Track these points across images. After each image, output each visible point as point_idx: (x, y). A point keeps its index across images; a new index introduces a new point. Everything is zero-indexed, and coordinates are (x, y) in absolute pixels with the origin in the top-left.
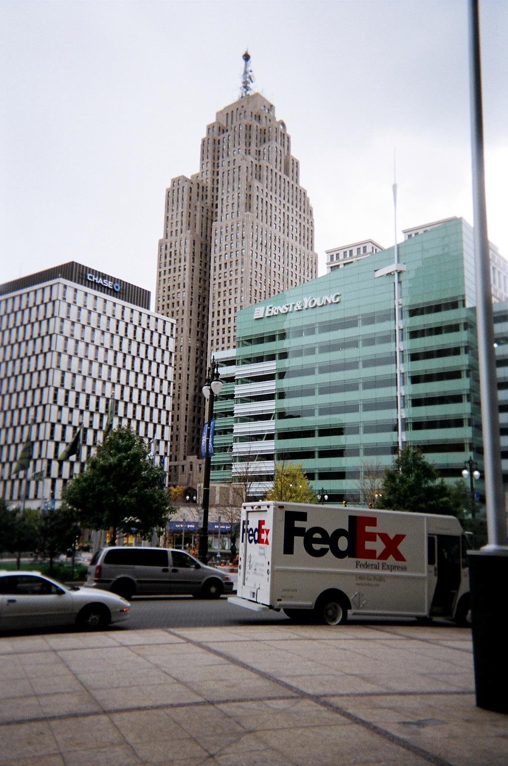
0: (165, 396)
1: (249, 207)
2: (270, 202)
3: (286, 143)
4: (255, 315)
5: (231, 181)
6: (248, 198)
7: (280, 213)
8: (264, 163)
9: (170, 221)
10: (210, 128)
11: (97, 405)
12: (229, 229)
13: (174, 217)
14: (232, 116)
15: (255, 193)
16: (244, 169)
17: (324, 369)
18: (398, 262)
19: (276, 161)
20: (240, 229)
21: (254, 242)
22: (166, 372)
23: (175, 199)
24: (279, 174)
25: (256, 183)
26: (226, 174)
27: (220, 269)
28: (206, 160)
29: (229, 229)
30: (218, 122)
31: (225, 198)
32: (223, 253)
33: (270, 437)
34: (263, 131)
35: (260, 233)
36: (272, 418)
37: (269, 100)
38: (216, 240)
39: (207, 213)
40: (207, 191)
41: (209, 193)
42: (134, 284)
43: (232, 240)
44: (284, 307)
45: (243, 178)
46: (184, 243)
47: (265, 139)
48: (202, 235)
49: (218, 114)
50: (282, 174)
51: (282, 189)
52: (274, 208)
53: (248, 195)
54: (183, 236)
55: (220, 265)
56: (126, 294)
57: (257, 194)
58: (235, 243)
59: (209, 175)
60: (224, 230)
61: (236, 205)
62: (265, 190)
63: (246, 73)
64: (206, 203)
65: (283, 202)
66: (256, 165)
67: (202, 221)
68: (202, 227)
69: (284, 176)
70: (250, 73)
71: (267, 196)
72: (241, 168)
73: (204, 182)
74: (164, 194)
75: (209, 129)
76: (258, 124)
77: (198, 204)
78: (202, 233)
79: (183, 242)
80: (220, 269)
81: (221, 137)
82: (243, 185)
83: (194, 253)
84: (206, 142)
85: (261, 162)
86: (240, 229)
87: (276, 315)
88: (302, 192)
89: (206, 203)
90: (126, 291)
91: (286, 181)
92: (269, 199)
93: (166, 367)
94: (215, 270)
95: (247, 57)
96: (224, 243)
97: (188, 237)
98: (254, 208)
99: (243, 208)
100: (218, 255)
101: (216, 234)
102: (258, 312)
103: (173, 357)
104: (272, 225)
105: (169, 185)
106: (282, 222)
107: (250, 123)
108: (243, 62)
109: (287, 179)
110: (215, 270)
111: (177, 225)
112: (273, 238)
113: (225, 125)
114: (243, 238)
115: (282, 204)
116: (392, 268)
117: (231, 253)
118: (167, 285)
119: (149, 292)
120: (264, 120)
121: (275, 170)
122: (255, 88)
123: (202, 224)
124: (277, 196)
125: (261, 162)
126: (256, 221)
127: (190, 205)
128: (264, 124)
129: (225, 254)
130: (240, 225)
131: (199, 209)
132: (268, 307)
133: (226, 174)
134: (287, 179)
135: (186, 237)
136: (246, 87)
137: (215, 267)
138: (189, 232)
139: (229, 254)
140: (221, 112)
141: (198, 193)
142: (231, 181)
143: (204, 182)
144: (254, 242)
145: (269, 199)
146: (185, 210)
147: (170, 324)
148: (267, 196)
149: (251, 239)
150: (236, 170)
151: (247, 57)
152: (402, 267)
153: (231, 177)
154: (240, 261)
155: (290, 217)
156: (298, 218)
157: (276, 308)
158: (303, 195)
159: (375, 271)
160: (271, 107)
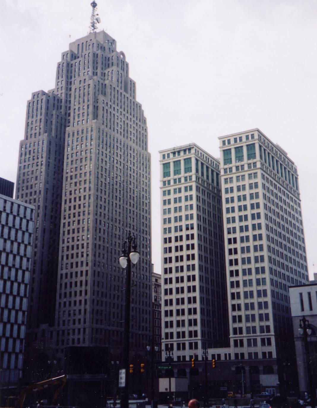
5: (82, 95)
10: (64, 55)
15: (101, 106)
16: (92, 86)
24: (120, 91)
25: (101, 98)
26: (78, 90)
28: (60, 79)
38: (68, 140)
41: (63, 104)
45: (91, 92)
48: (57, 137)
50: (122, 91)
59: (64, 91)
62: (109, 103)
63: (93, 16)
64: (61, 112)
66: (102, 84)
69: (124, 93)
77: (54, 112)
78: (57, 136)
79: (41, 143)
88: (138, 106)
95: (94, 5)
96: (75, 143)
99: (91, 116)
105: (30, 97)
113: (76, 52)
114: (91, 140)
127: (47, 113)
131: (54, 116)
133: (78, 90)
138: (46, 134)
140: (74, 43)
141: (54, 104)
146: (43, 117)
150: (86, 87)
151: (94, 5)
153: (82, 92)
160: (113, 42)
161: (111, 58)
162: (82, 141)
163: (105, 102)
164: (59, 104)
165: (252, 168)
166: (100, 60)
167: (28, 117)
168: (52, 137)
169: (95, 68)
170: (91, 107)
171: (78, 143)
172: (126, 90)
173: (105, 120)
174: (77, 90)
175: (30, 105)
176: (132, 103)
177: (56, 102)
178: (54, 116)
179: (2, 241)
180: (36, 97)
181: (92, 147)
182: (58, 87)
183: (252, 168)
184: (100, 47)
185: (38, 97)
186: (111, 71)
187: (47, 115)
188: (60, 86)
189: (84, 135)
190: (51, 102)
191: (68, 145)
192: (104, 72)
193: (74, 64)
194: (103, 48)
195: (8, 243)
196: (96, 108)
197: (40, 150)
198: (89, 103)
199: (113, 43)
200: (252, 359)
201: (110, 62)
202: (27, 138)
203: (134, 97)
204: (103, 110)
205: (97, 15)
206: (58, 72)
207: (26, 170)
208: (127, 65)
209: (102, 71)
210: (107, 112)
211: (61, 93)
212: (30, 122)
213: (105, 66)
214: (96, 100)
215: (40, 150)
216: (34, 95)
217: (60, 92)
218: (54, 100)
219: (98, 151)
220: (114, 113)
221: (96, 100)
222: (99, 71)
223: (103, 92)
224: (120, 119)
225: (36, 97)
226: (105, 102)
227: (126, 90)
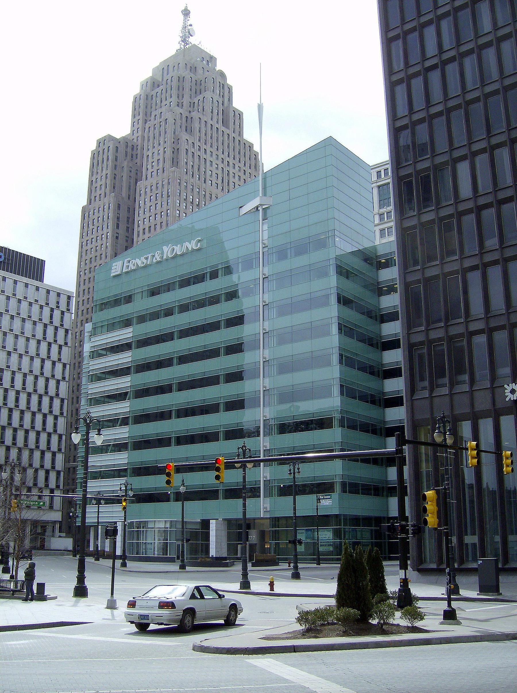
0: (58, 382)
1: (175, 162)
2: (209, 158)
3: (226, 94)
4: (112, 271)
5: (157, 135)
6: (175, 153)
7: (217, 168)
8: (195, 115)
9: (94, 185)
10: (144, 85)
11: (28, 402)
12: (154, 188)
13: (99, 180)
14: (168, 70)
15: (183, 146)
16: (171, 121)
17: (186, 333)
18: (265, 194)
19: (212, 112)
20: (166, 187)
21: (182, 200)
22: (60, 353)
23: (100, 162)
24: (216, 126)
25: (185, 136)
26: (152, 129)
27: (144, 233)
28: (137, 118)
29: (154, 188)
30: (152, 78)
31: (150, 155)
32: (147, 215)
33: (125, 422)
34: (181, 79)
35: (183, 187)
36: (127, 398)
37: (208, 52)
38: (140, 201)
39: (137, 174)
40: (137, 149)
42: (12, 248)
43: (156, 200)
44: (143, 259)
45: (170, 131)
46: (108, 208)
47: (201, 90)
48: (129, 198)
49: (154, 70)
50: (220, 126)
51: (226, 144)
52: (208, 163)
53: (176, 149)
54: (106, 200)
55: (144, 229)
56: (12, 264)
57: (187, 147)
58: (159, 203)
60: (148, 190)
61: (161, 161)
62: (197, 144)
63: (185, 27)
64: (137, 163)
65: (221, 156)
66: (187, 117)
67: (130, 182)
68: (129, 189)
69: (223, 129)
70: (189, 27)
71: (199, 150)
72: (167, 121)
73: (135, 140)
74: (89, 156)
75: (142, 86)
76: (192, 75)
77: (125, 164)
78: (129, 196)
79: (106, 207)
80: (144, 233)
81: (154, 93)
82: (169, 137)
83: (118, 218)
84: (138, 99)
85: (193, 114)
86: (166, 187)
87: (135, 270)
88: (247, 146)
89: (137, 163)
90: (12, 260)
91: (225, 134)
92: (202, 153)
93: (60, 347)
94: (138, 235)
95: (186, 13)
96: (148, 204)
97: (112, 200)
98: (182, 163)
99: (168, 163)
100: (141, 218)
101: (140, 195)
102: (115, 267)
103: (70, 335)
104: (207, 181)
105: (94, 146)
106: (220, 179)
107: (183, 75)
108: (182, 17)
109: (227, 131)
110: (138, 235)
111: (101, 189)
112: (208, 196)
113: (161, 80)
114: (168, 196)
115: (220, 158)
116: (256, 202)
117: (155, 215)
118: (88, 257)
119: (45, 261)
120: (200, 71)
121: (210, 122)
122: (192, 40)
123: (130, 186)
124: (214, 150)
125: (193, 114)
126: (185, 177)
127: (116, 166)
128: (200, 75)
129: (150, 217)
130: (166, 181)
131: (125, 169)
132: (126, 261)
133: (152, 129)
134: (227, 131)
135: (110, 200)
136: (184, 40)
137: (139, 232)
138: (113, 194)
139: (153, 216)
141: (126, 152)
142: (157, 135)
143: (135, 140)
144: (182, 200)
145: (202, 153)
146: (109, 172)
147: (66, 297)
148: (199, 150)
149: (178, 197)
150: (163, 124)
151: (186, 13)
152: (268, 201)
153: (157, 131)
154: (164, 224)
155: (231, 173)
156: (241, 174)
157: (133, 261)
158: (248, 149)
159: (241, 207)
160: (212, 59)
161: (203, 81)
162: (156, 200)
163: (190, 142)
164: (134, 153)
165: (386, 219)
166: (187, 86)
167: (92, 173)
168: (123, 198)
169: (180, 97)
170: (169, 151)
171: (151, 204)
172: (225, 123)
173: (190, 167)
174: (151, 129)
175: (95, 156)
176: (237, 142)
177: (129, 150)
178: (125, 169)
179: (4, 355)
180: (101, 145)
181: (169, 207)
182: (134, 128)
183: (386, 219)
184: (188, 67)
185: (104, 144)
186: (202, 99)
187: (115, 169)
188: (136, 126)
189: (159, 191)
190: (122, 149)
191: (140, 207)
192: (192, 102)
193: (155, 95)
194: (193, 69)
195: (14, 357)
196: (176, 151)
197: (106, 217)
198: (165, 145)
199: (211, 61)
200: (449, 483)
201: (202, 87)
202: (90, 201)
203: (240, 134)
204: (187, 153)
205: (191, 25)
206: (134, 109)
207: (89, 246)
208: (230, 89)
209: (190, 100)
210: (193, 156)
211: (138, 137)
212: (94, 180)
213: (196, 93)
214: (176, 141)
215: (106, 217)
216: (99, 142)
217: (136, 135)
218: (127, 147)
219: (178, 212)
220: (205, 156)
221: (176, 141)
222: (186, 100)
223: (189, 128)
224: (237, 168)
225: (101, 145)
226: (190, 142)
227: (225, 123)
